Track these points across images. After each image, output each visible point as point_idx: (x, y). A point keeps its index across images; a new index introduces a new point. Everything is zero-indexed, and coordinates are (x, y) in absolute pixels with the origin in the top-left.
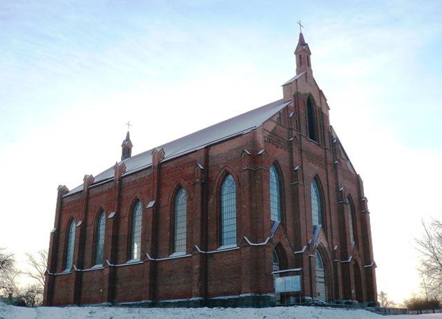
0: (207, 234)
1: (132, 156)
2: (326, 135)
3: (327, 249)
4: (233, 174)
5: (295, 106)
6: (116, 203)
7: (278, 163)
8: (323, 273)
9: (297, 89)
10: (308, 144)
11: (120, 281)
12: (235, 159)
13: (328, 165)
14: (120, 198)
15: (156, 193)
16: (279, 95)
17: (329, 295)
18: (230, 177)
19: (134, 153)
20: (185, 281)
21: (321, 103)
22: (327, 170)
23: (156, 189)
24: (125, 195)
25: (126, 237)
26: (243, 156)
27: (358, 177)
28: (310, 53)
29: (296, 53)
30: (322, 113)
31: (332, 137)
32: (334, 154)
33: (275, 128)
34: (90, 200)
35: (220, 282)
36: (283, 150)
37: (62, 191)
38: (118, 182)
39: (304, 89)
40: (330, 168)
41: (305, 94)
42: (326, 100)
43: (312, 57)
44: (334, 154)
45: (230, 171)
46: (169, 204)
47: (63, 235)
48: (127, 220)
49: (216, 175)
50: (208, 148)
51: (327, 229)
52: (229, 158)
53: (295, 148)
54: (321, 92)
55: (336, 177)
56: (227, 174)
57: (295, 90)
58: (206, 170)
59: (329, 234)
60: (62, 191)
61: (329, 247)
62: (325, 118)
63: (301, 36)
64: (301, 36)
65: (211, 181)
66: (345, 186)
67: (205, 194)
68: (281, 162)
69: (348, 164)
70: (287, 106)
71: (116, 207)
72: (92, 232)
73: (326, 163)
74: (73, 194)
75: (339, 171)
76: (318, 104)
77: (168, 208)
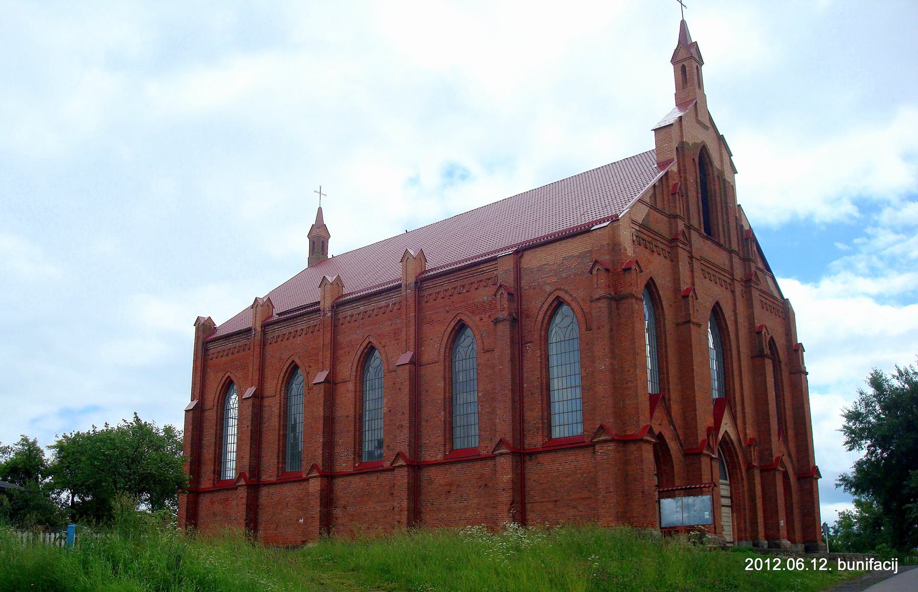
0: (522, 415)
1: (330, 256)
2: (733, 224)
3: (736, 443)
4: (574, 304)
5: (679, 170)
6: (328, 354)
7: (654, 283)
8: (728, 488)
9: (682, 136)
10: (699, 244)
11: (342, 502)
12: (575, 275)
13: (736, 283)
14: (335, 346)
15: (412, 336)
16: (649, 143)
17: (739, 530)
18: (565, 309)
19: (335, 248)
20: (478, 504)
21: (722, 161)
22: (733, 292)
23: (412, 329)
24: (343, 339)
25: (352, 418)
26: (594, 272)
27: (786, 302)
28: (701, 62)
29: (674, 61)
30: (724, 180)
31: (742, 226)
32: (746, 260)
33: (648, 215)
34: (269, 349)
35: (550, 506)
36: (662, 257)
37: (205, 328)
38: (329, 314)
39: (694, 136)
40: (739, 288)
41: (695, 144)
42: (730, 155)
43: (704, 69)
44: (746, 260)
45: (567, 298)
46: (442, 357)
47: (211, 415)
48: (351, 386)
49: (537, 305)
50: (521, 251)
51: (735, 406)
52: (564, 275)
53: (683, 255)
54: (721, 139)
55: (750, 305)
56: (559, 303)
57: (679, 139)
58: (516, 295)
59: (739, 414)
60: (205, 328)
61: (739, 440)
62: (728, 190)
63: (683, 25)
64: (683, 25)
65: (528, 316)
66: (763, 318)
67: (518, 343)
68: (659, 282)
69: (769, 279)
70: (667, 173)
71: (328, 363)
72: (276, 410)
73: (733, 280)
74: (227, 337)
75: (756, 294)
76: (716, 163)
77: (439, 368)
